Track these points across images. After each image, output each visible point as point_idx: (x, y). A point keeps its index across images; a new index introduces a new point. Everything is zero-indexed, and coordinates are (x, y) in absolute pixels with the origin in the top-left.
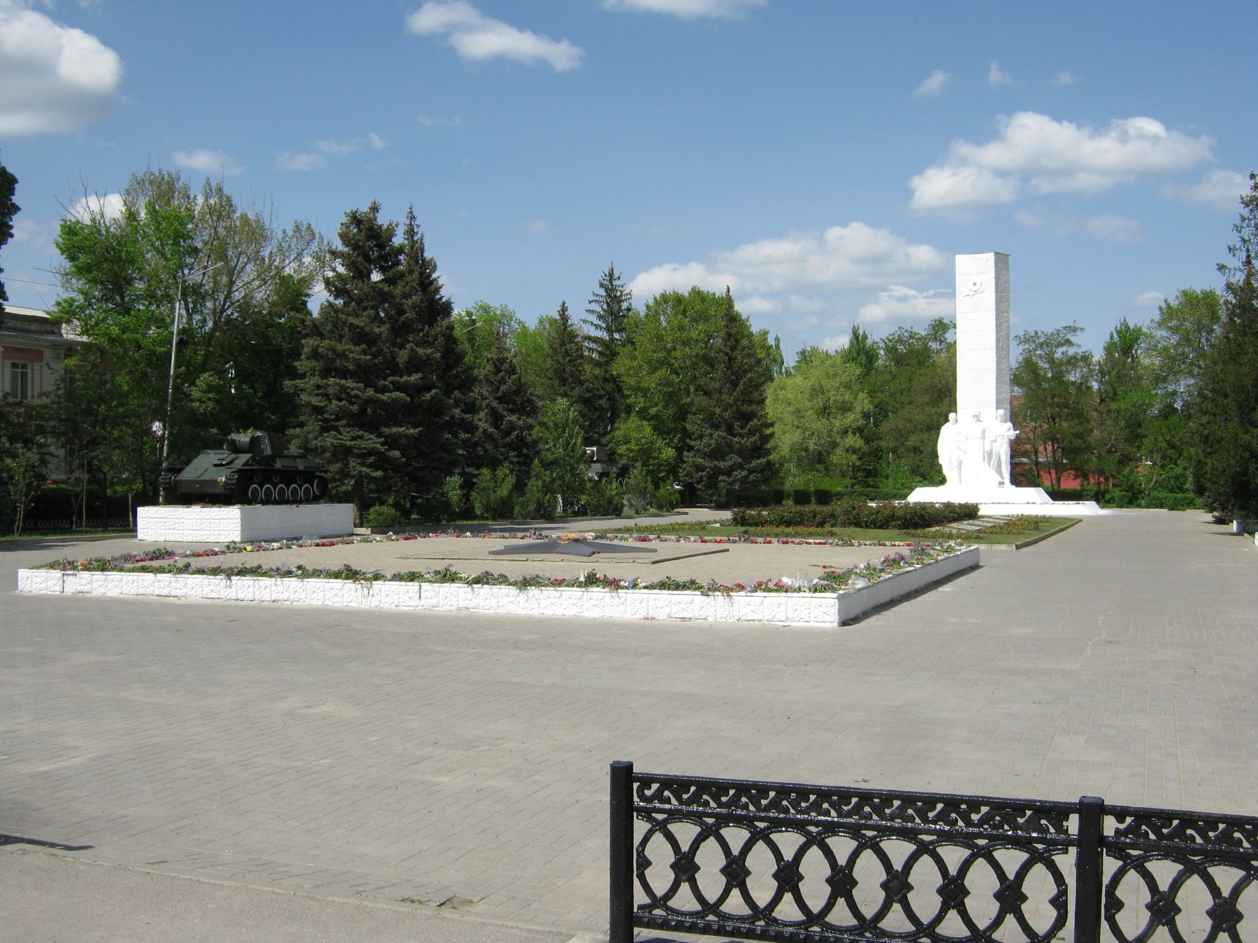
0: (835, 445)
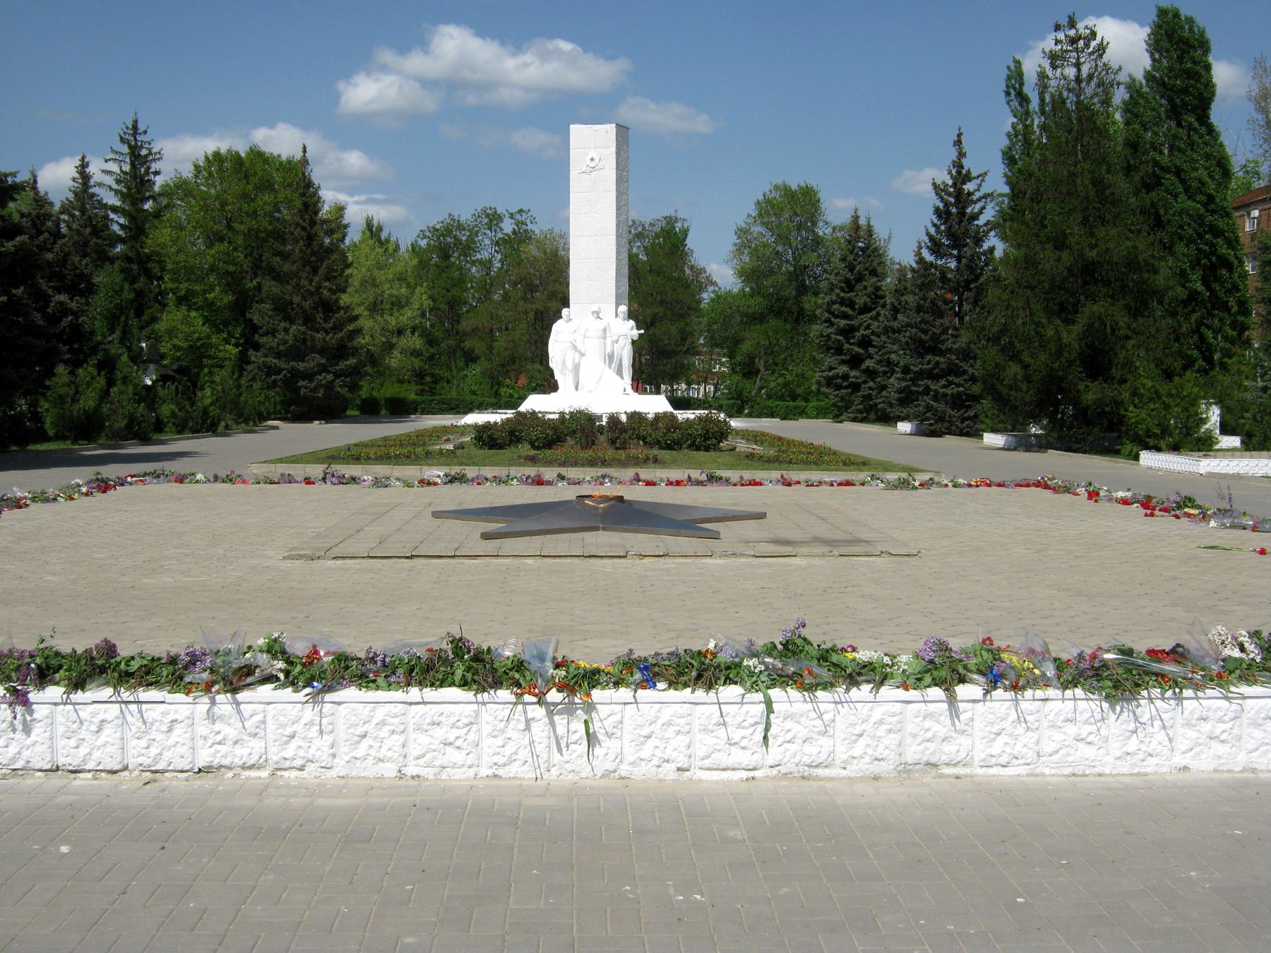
0: (391, 346)
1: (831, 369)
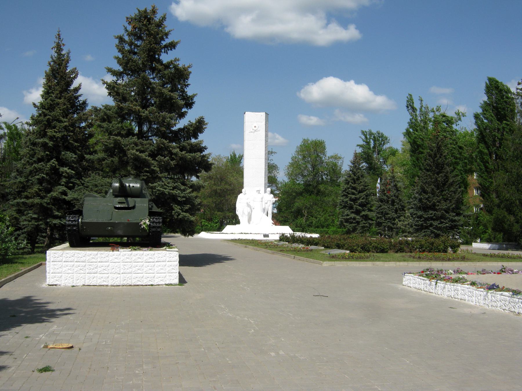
1: (348, 215)
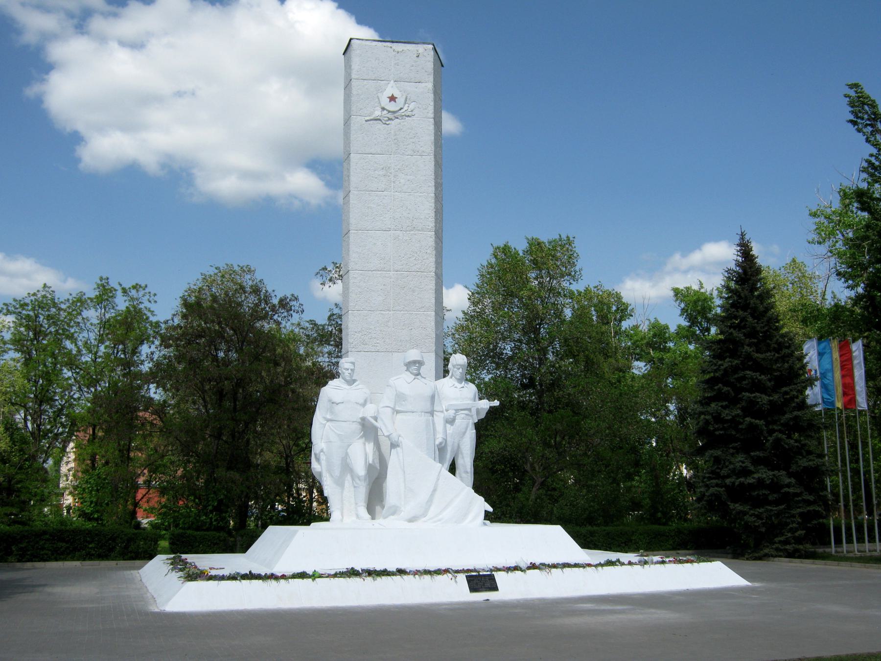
1: (745, 472)
